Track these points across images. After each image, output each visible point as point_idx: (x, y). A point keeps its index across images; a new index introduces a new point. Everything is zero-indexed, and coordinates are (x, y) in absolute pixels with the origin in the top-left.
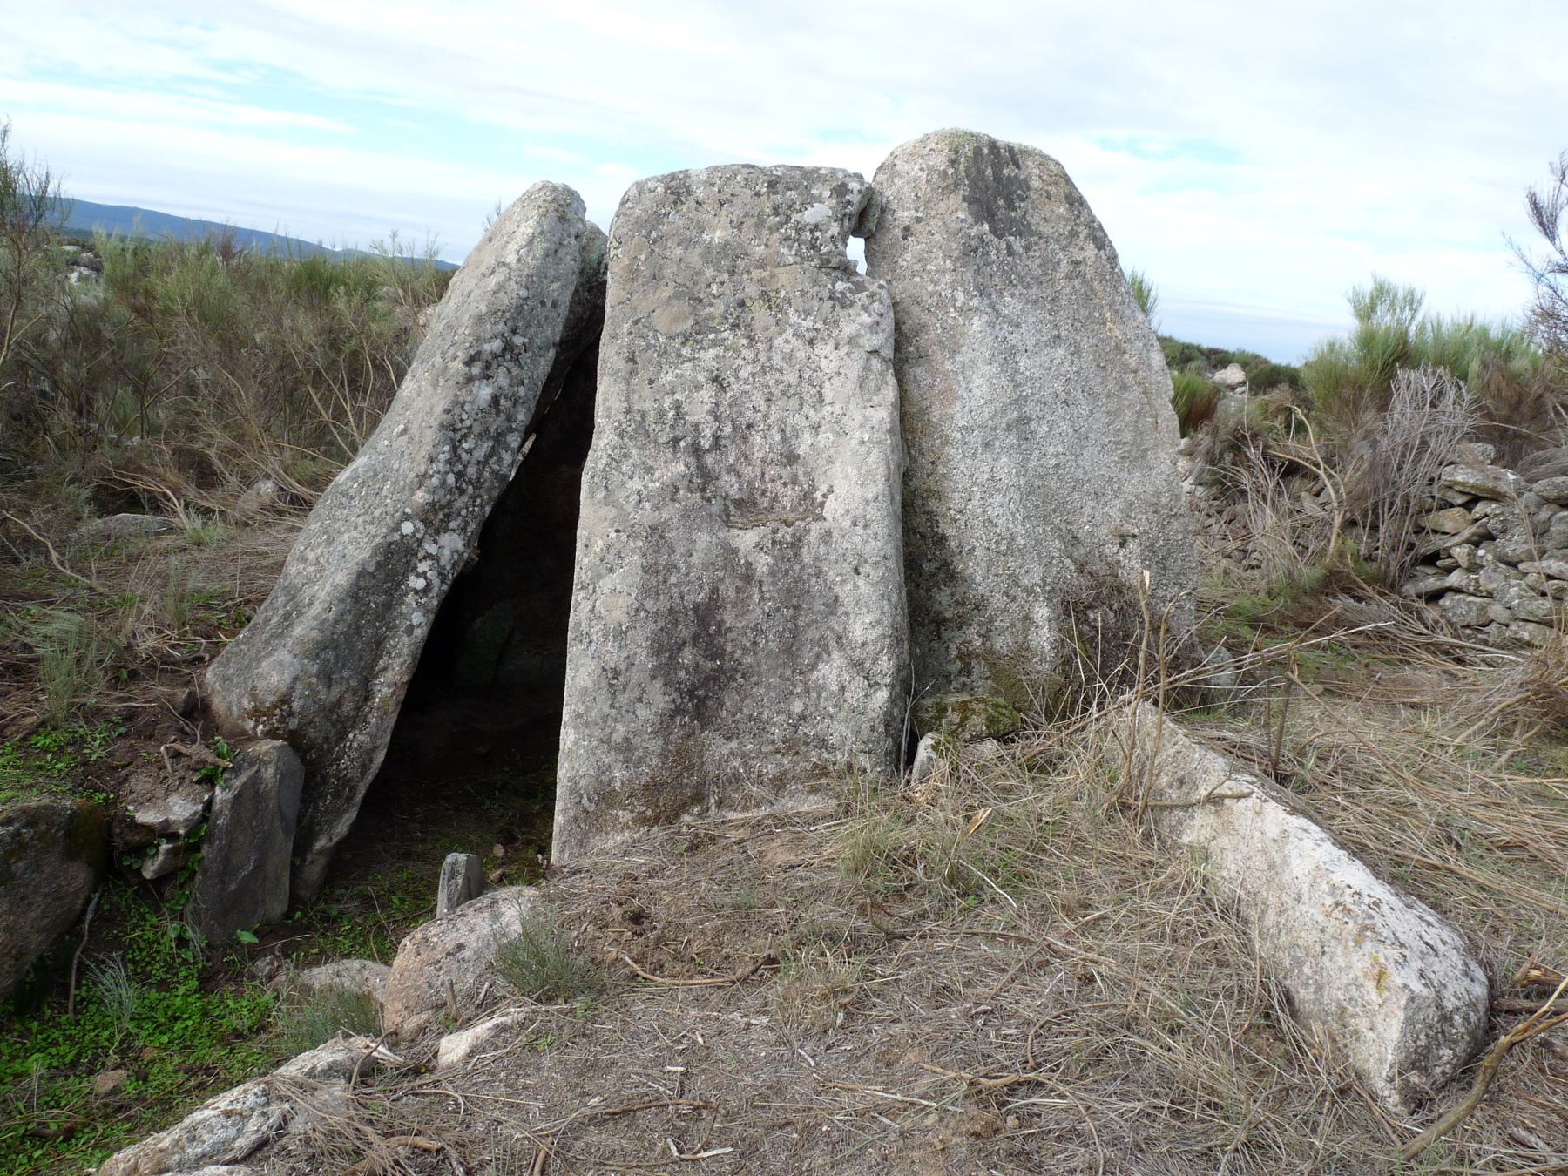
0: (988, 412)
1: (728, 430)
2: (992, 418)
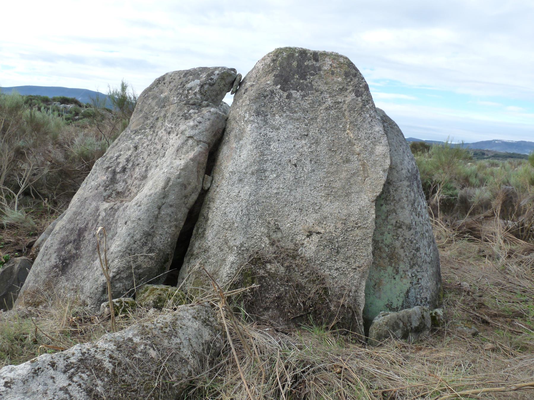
0: (244, 165)
1: (130, 165)
2: (245, 169)
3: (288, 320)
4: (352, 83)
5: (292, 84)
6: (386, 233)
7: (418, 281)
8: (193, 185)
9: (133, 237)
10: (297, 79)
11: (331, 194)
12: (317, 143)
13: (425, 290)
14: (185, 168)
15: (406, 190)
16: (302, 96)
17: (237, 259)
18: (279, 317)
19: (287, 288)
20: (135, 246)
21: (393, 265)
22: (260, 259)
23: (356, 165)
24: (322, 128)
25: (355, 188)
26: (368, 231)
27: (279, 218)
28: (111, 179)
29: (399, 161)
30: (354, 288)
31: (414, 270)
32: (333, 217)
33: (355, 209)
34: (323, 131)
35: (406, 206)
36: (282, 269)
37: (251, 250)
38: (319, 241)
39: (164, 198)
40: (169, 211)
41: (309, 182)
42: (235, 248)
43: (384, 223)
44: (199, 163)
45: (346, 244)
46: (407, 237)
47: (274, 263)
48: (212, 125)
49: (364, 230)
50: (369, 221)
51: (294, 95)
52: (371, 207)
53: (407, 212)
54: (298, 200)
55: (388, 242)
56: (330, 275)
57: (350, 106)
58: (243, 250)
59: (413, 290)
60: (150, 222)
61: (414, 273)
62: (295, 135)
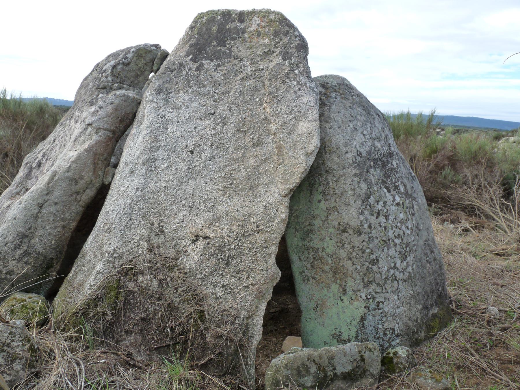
3: (150, 350)
4: (281, 43)
5: (207, 53)
6: (327, 238)
7: (378, 306)
8: (87, 179)
9: (5, 238)
10: (214, 46)
11: (230, 187)
12: (224, 122)
13: (390, 318)
14: (79, 158)
15: (353, 181)
16: (216, 66)
17: (105, 268)
18: (141, 345)
19: (158, 308)
20: (6, 248)
21: (338, 281)
22: (132, 268)
23: (270, 148)
24: (233, 103)
25: (265, 179)
26: (272, 237)
27: (165, 219)
28: (27, 175)
29: (342, 141)
30: (244, 313)
31: (370, 290)
32: (229, 217)
33: (259, 206)
34: (234, 107)
35: (352, 202)
36: (155, 283)
37: (125, 257)
38: (204, 248)
39: (47, 194)
40: (53, 209)
41: (205, 172)
42: (107, 254)
43: (323, 225)
44: (95, 154)
45: (241, 253)
46: (356, 244)
47: (146, 275)
48: (116, 110)
49: (267, 235)
50: (275, 224)
51: (206, 66)
52: (281, 204)
53: (353, 211)
54: (188, 196)
55: (330, 250)
56: (212, 293)
57: (272, 73)
58: (115, 258)
59: (371, 317)
60: (27, 222)
61: (370, 293)
62: (199, 114)
